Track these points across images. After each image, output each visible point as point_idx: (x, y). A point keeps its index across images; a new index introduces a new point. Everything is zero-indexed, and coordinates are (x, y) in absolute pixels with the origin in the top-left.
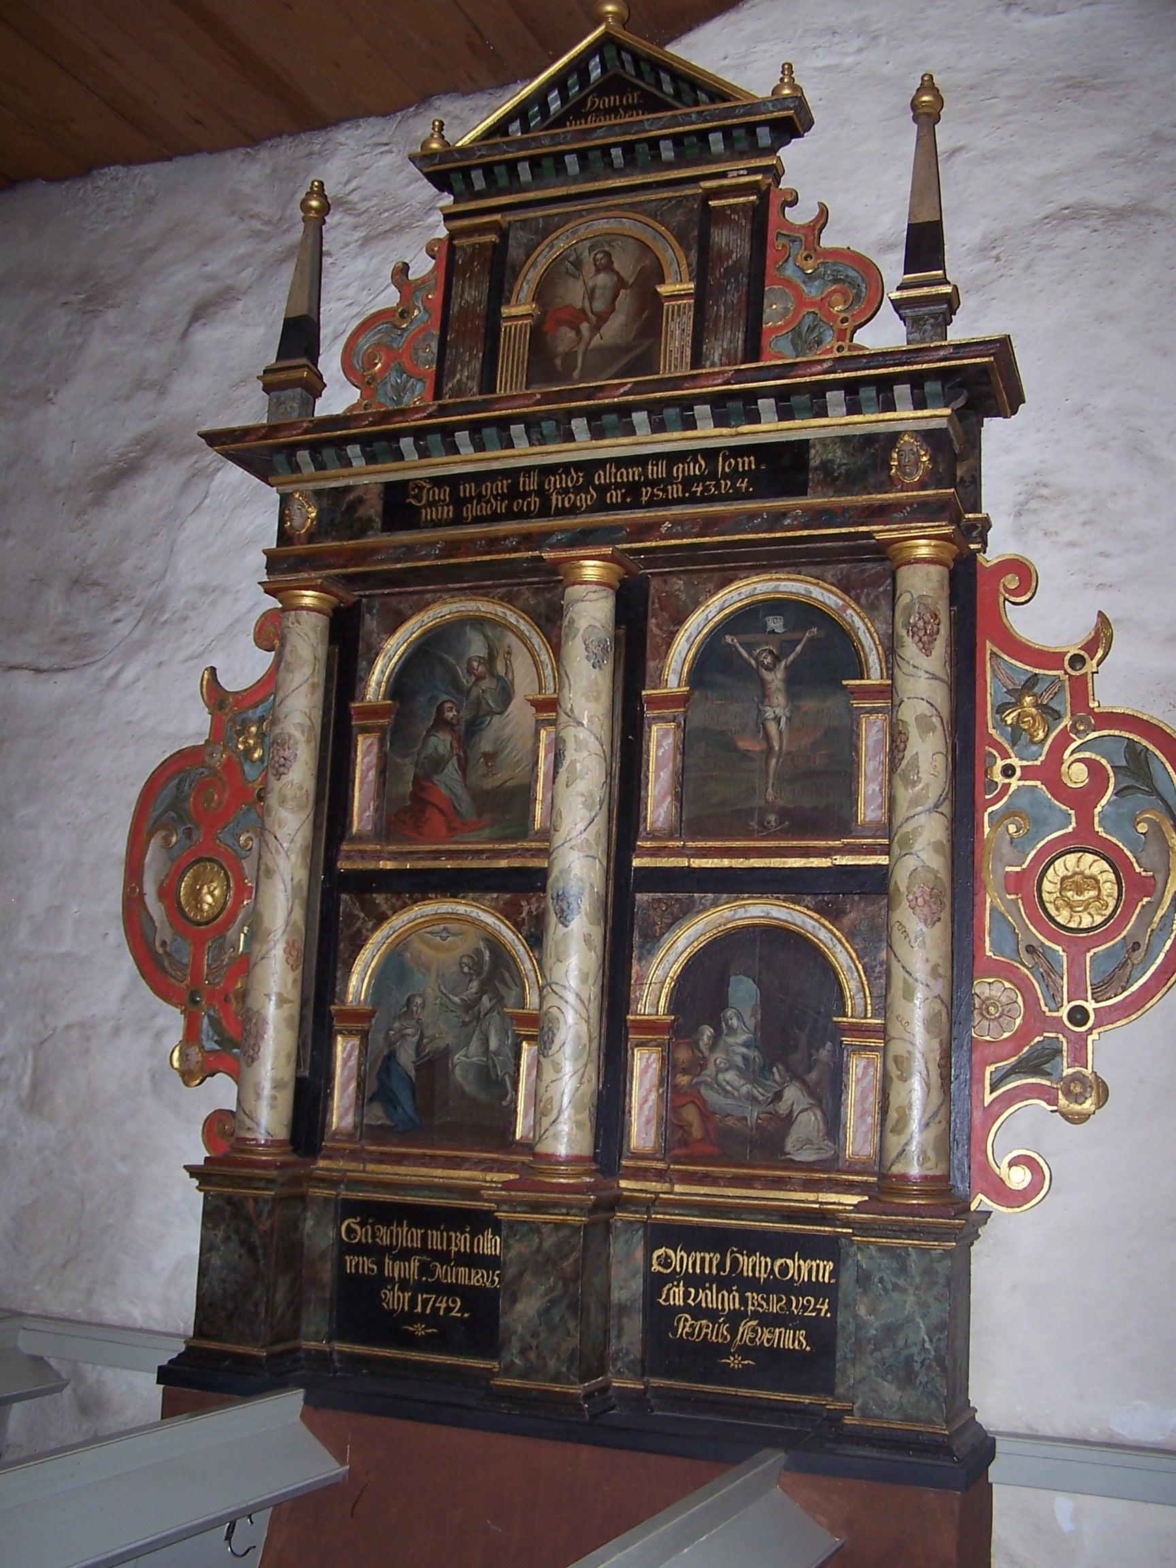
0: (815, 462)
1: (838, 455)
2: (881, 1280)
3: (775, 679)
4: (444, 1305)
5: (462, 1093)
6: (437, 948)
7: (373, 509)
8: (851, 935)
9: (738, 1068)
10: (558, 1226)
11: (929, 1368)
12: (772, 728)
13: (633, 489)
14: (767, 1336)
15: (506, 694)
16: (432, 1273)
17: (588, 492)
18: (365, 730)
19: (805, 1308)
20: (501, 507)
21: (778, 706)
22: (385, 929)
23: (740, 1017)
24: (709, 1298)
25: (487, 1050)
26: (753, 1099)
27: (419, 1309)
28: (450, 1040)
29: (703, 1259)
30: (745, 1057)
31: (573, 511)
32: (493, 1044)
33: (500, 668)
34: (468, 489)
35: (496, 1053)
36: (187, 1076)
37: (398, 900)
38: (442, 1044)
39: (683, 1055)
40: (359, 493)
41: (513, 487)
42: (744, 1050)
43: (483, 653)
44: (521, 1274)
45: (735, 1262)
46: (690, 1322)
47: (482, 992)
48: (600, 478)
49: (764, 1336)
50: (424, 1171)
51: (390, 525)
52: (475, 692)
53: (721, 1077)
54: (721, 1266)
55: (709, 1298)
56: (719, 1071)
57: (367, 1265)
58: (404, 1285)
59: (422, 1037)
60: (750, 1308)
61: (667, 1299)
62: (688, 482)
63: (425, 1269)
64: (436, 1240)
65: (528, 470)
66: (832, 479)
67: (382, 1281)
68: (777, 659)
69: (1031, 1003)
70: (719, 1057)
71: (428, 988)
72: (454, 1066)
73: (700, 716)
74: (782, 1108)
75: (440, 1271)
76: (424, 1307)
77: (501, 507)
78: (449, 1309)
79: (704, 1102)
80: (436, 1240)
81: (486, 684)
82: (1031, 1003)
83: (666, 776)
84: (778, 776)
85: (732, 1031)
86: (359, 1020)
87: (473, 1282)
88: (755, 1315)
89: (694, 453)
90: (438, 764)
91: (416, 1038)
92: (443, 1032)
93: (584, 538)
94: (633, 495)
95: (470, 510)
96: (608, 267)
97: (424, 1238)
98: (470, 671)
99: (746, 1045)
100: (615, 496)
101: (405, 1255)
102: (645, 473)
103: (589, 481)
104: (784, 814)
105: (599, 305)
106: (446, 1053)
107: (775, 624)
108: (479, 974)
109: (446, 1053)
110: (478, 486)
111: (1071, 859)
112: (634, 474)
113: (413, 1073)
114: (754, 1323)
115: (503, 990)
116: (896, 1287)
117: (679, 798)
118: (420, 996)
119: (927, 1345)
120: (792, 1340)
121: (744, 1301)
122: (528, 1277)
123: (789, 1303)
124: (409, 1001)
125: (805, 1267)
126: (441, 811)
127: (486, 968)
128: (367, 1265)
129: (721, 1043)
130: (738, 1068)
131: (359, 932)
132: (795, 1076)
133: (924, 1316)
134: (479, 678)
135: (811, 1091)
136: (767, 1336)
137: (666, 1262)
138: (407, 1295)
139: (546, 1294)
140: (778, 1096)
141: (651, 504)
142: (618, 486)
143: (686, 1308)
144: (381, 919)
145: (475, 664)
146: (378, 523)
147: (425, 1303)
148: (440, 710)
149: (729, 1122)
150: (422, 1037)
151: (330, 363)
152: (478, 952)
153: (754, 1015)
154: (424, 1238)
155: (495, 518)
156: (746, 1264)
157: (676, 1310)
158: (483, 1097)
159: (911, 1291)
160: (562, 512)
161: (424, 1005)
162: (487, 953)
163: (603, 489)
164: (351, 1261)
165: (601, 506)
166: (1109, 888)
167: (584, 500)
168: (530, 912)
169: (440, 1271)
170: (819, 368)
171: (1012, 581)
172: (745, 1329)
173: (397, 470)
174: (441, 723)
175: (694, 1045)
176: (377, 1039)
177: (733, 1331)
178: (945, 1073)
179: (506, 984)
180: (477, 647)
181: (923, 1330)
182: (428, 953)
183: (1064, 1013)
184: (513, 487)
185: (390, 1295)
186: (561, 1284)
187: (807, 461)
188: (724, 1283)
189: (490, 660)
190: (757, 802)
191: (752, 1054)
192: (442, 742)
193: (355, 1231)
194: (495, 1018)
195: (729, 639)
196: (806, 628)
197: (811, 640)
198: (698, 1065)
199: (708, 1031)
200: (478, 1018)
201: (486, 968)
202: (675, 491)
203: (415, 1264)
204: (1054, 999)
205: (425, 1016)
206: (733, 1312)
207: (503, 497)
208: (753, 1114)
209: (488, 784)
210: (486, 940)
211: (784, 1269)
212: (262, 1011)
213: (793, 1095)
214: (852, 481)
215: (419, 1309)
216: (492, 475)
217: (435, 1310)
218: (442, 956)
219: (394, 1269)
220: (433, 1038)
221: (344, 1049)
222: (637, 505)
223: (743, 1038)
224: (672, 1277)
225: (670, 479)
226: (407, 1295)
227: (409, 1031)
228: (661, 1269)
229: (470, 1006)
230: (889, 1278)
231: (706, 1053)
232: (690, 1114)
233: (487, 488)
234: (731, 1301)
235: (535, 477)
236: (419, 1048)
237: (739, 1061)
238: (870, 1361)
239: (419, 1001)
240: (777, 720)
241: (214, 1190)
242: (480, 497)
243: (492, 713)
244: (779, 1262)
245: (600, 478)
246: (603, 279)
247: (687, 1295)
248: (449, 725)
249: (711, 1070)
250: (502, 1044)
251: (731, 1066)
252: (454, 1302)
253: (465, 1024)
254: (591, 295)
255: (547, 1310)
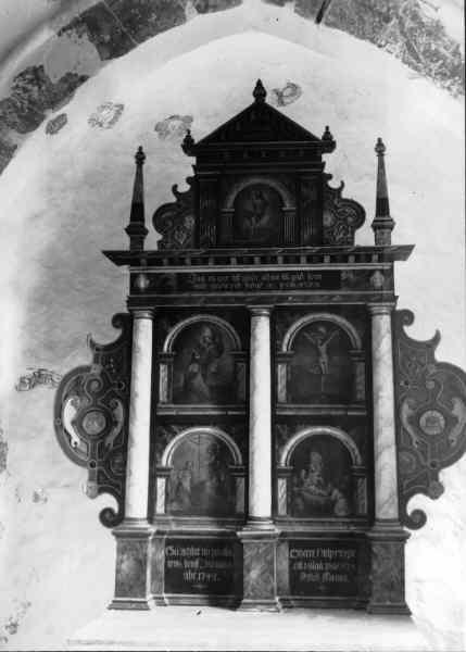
1: (351, 276)
7: (173, 283)
10: (265, 544)
12: (322, 366)
16: (204, 565)
21: (324, 358)
22: (177, 438)
24: (312, 566)
31: (255, 290)
32: (222, 479)
36: (93, 497)
37: (319, 485)
48: (264, 278)
51: (181, 290)
55: (312, 566)
57: (177, 564)
58: (193, 570)
62: (297, 282)
66: (348, 284)
67: (183, 570)
68: (323, 341)
69: (418, 462)
73: (295, 362)
74: (333, 497)
82: (418, 462)
83: (284, 382)
93: (260, 301)
96: (260, 196)
98: (205, 341)
101: (192, 558)
105: (259, 211)
111: (429, 412)
112: (277, 277)
124: (187, 463)
128: (177, 564)
132: (335, 486)
140: (330, 494)
141: (284, 289)
143: (303, 570)
144: (175, 434)
151: (149, 225)
155: (223, 290)
160: (250, 290)
163: (265, 282)
164: (170, 563)
166: (442, 422)
171: (406, 318)
174: (194, 360)
175: (299, 477)
176: (174, 478)
183: (428, 464)
191: (321, 478)
192: (195, 368)
198: (301, 483)
199: (304, 472)
203: (197, 563)
204: (426, 459)
214: (355, 286)
221: (161, 482)
222: (278, 289)
223: (317, 473)
224: (299, 560)
225: (290, 281)
232: (299, 501)
233: (220, 279)
234: (319, 567)
236: (192, 481)
241: (400, 604)
245: (264, 278)
246: (259, 201)
248: (197, 361)
249: (306, 485)
254: (255, 207)
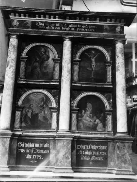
0: (105, 28)
2: (121, 147)
3: (93, 60)
4: (38, 157)
5: (40, 121)
6: (35, 97)
8: (106, 97)
9: (88, 117)
11: (129, 161)
12: (93, 67)
13: (76, 28)
14: (96, 158)
15: (48, 58)
17: (68, 28)
18: (22, 61)
19: (102, 154)
20: (53, 28)
21: (94, 63)
23: (89, 109)
25: (45, 114)
26: (91, 121)
27: (33, 158)
28: (38, 112)
29: (85, 147)
30: (90, 115)
31: (66, 30)
32: (46, 112)
33: (47, 54)
34: (47, 24)
35: (47, 114)
38: (36, 113)
39: (80, 115)
40: (27, 21)
41: (55, 25)
42: (89, 114)
43: (44, 51)
44: (60, 149)
45: (91, 147)
46: (83, 157)
47: (44, 104)
48: (70, 26)
49: (96, 158)
50: (111, 122)
52: (42, 57)
53: (86, 118)
54: (88, 147)
56: (86, 117)
58: (30, 154)
59: (32, 111)
60: (93, 154)
61: (79, 153)
62: (85, 28)
63: (34, 151)
64: (37, 145)
65: (58, 23)
66: (106, 30)
68: (93, 57)
70: (85, 115)
71: (34, 104)
72: (39, 116)
74: (96, 123)
75: (37, 151)
76: (34, 158)
77: (53, 28)
78: (39, 158)
79: (83, 122)
80: (37, 145)
81: (44, 56)
84: (94, 74)
85: (88, 111)
86: (21, 109)
87: (44, 152)
88: (94, 155)
89: (86, 24)
90: (36, 67)
91: (31, 112)
92: (36, 111)
94: (76, 29)
95: (48, 28)
97: (35, 145)
98: (41, 53)
99: (90, 113)
100: (73, 29)
101: (31, 148)
102: (78, 26)
103: (68, 26)
104: (94, 79)
106: (37, 114)
107: (93, 52)
108: (43, 101)
109: (37, 114)
110: (82, 26)
113: (31, 117)
114: (94, 156)
115: (48, 104)
116: (124, 149)
117: (79, 76)
118: (33, 105)
119: (129, 157)
120: (101, 159)
121: (92, 153)
122: (61, 149)
123: (100, 153)
124: (30, 105)
125: (102, 147)
126: (36, 75)
127: (45, 101)
129: (86, 113)
130: (88, 117)
131: (21, 94)
133: (128, 153)
134: (43, 55)
135: (100, 120)
136: (96, 158)
137: (79, 147)
138: (31, 155)
139: (65, 152)
140: (95, 121)
141: (79, 31)
142: (73, 28)
145: (42, 53)
146: (31, 27)
147: (34, 157)
148: (36, 59)
149: (87, 125)
150: (32, 111)
152: (43, 98)
153: (91, 109)
154: (35, 145)
156: (93, 147)
157: (82, 155)
158: (44, 121)
159: (126, 149)
161: (33, 106)
162: (45, 98)
163: (71, 28)
165: (70, 30)
167: (68, 29)
168: (53, 92)
169: (37, 151)
170: (32, 10)
172: (93, 158)
173: (34, 19)
175: (81, 113)
177: (91, 158)
178: (32, 132)
179: (48, 103)
180: (43, 50)
181: (128, 155)
182: (33, 98)
184: (55, 25)
185: (27, 156)
186: (67, 150)
187: (103, 28)
188: (89, 150)
189: (45, 52)
190: (90, 77)
191: (91, 115)
193: (21, 145)
194: (47, 108)
195: (86, 53)
196: (98, 53)
197: (99, 55)
198: (82, 116)
199: (83, 111)
200: (43, 109)
201: (45, 101)
202: (82, 30)
203: (33, 150)
205: (33, 108)
206: (91, 155)
207: (53, 26)
208: (91, 124)
209: (45, 71)
210: (45, 96)
211: (99, 148)
212: (127, 95)
213: (97, 121)
215: (33, 158)
216: (52, 23)
217: (37, 158)
218: (37, 98)
219: (27, 151)
220: (34, 112)
222: (76, 31)
225: (82, 28)
226: (31, 155)
227: (30, 110)
228: (78, 148)
229: (41, 106)
230: (122, 147)
231: (83, 114)
234: (90, 153)
235: (59, 24)
236: (32, 113)
237: (89, 116)
238: (120, 160)
239: (32, 105)
240: (94, 66)
242: (49, 26)
243: (46, 60)
244: (98, 147)
247: (83, 152)
248: (37, 62)
250: (47, 112)
251: (87, 116)
252: (40, 156)
253: (41, 109)
255: (65, 154)
